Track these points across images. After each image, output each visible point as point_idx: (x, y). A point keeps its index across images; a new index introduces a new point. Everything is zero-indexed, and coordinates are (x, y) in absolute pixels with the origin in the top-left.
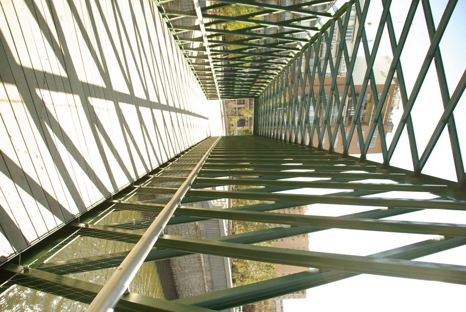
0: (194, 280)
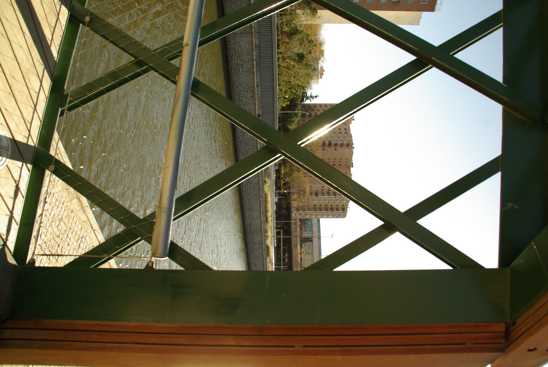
0: (243, 44)
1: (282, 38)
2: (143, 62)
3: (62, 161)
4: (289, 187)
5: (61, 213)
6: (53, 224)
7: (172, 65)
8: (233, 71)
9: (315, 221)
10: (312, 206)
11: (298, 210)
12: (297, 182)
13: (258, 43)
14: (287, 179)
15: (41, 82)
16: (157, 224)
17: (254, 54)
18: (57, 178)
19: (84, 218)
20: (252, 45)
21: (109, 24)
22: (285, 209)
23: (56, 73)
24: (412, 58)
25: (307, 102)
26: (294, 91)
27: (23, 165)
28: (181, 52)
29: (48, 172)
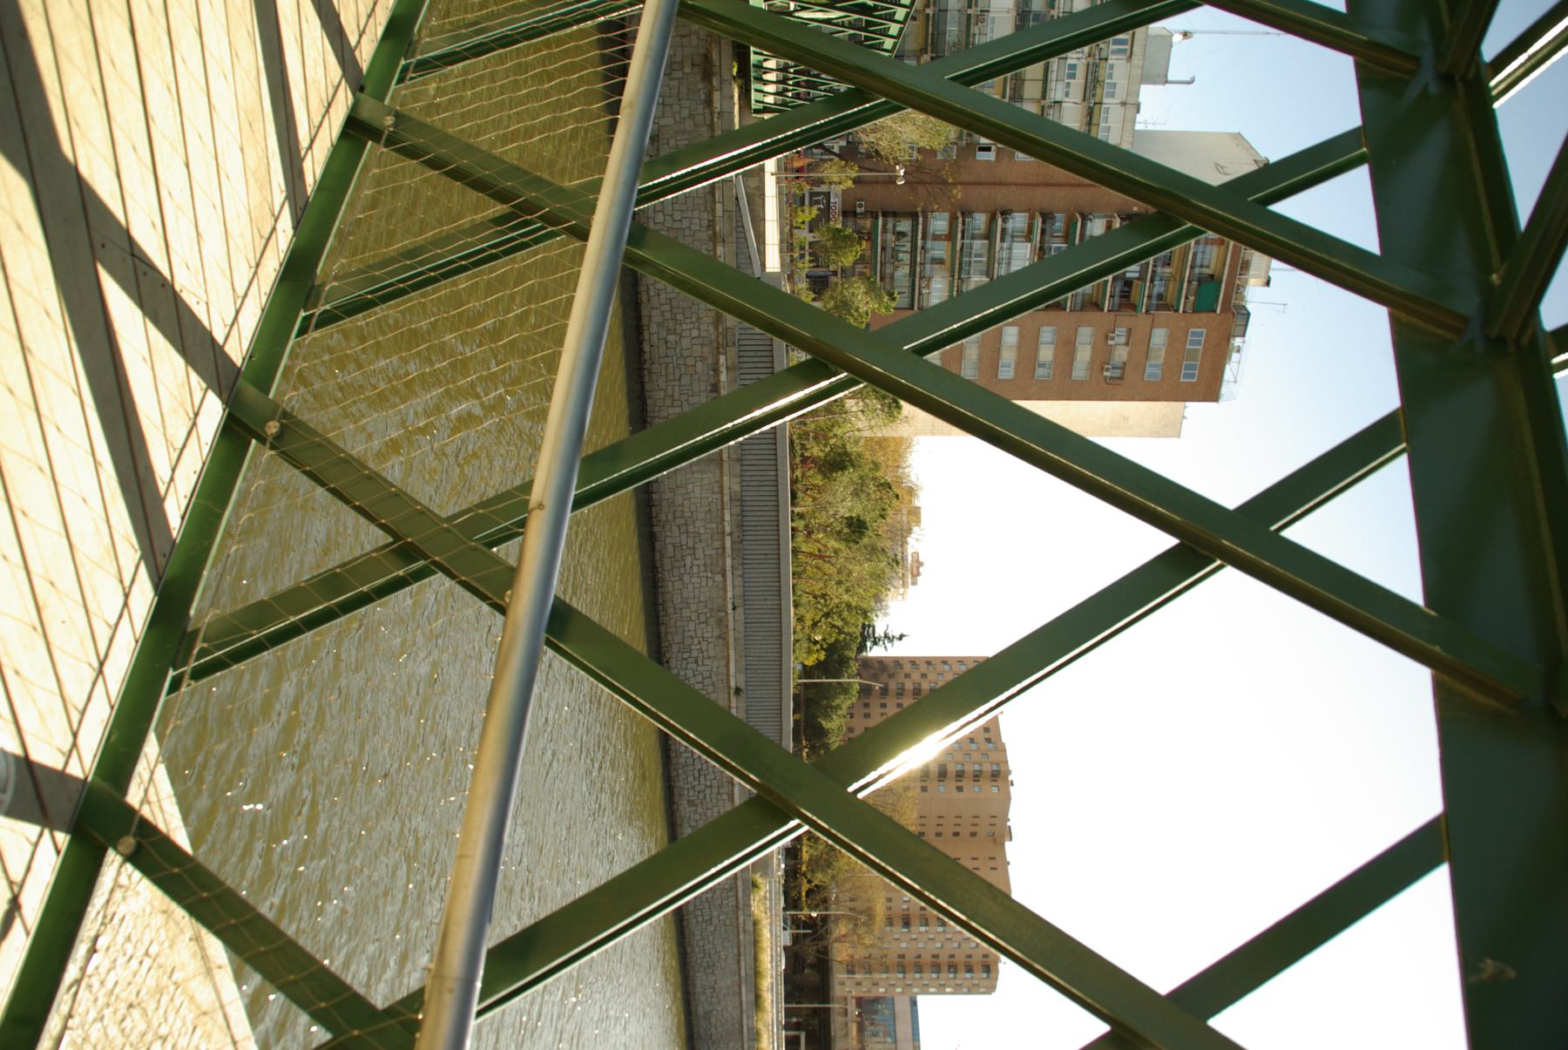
0: (697, 490)
1: (803, 474)
2: (412, 551)
3: (162, 827)
4: (825, 901)
5: (139, 979)
6: (107, 1012)
7: (496, 561)
8: (667, 566)
9: (902, 1006)
10: (893, 958)
11: (851, 971)
12: (848, 886)
13: (737, 488)
14: (819, 878)
15: (127, 596)
16: (427, 1027)
17: (727, 518)
18: (137, 874)
19: (205, 997)
20: (722, 493)
21: (330, 443)
22: (811, 966)
23: (171, 570)
24: (1167, 541)
25: (875, 652)
26: (839, 623)
27: (41, 835)
28: (523, 524)
29: (113, 859)
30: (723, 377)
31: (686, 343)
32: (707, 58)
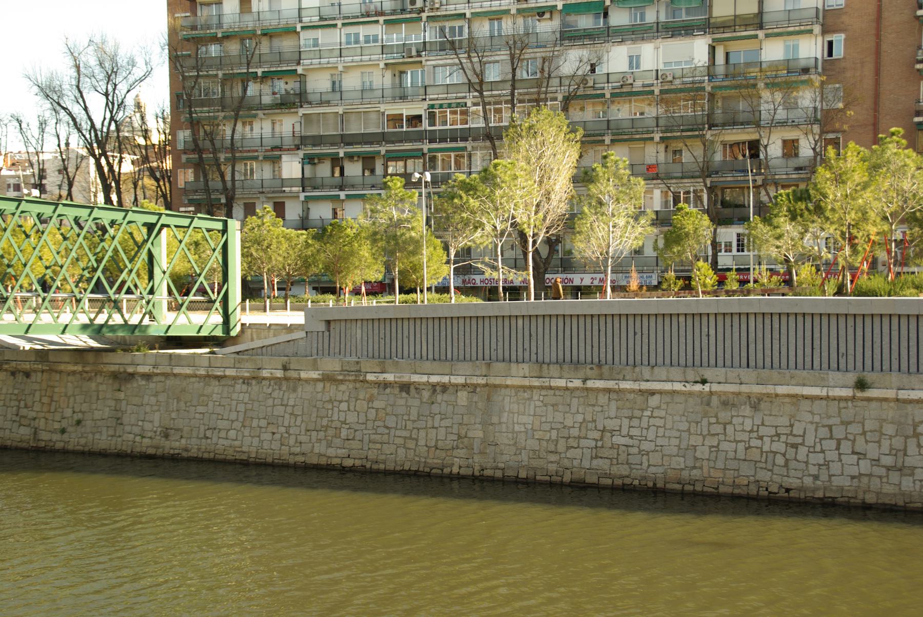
0: (524, 419)
8: (624, 470)
13: (525, 368)
17: (562, 383)
20: (531, 388)
30: (390, 377)
31: (352, 418)
32: (115, 376)
